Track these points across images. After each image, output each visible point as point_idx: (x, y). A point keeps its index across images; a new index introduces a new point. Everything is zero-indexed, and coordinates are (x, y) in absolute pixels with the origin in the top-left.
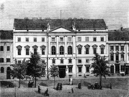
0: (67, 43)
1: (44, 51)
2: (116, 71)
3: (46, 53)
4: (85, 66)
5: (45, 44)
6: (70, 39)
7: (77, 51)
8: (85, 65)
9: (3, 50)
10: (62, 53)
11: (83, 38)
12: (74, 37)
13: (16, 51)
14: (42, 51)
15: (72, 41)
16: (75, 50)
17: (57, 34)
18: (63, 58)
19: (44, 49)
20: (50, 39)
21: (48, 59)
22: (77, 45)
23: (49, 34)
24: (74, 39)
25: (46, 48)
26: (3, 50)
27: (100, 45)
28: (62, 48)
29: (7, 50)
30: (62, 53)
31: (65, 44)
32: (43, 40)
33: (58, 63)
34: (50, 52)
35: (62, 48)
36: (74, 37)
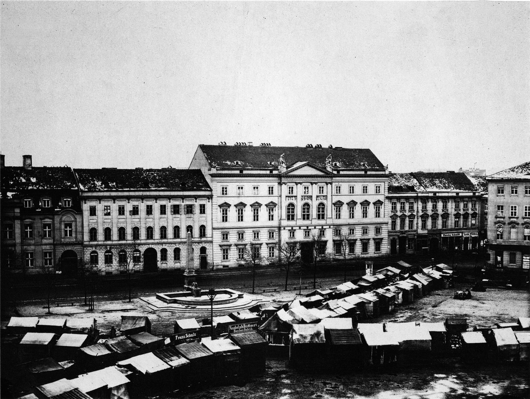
0: (317, 196)
1: (271, 213)
2: (162, 260)
3: (276, 218)
4: (266, 246)
5: (275, 200)
6: (321, 189)
7: (334, 213)
8: (267, 244)
9: (204, 213)
10: (306, 216)
11: (345, 187)
12: (329, 185)
13: (219, 214)
14: (270, 213)
15: (325, 194)
16: (330, 211)
17: (298, 180)
18: (309, 228)
19: (272, 210)
20: (285, 189)
21: (282, 228)
22: (333, 202)
23: (284, 180)
24: (328, 190)
25: (277, 206)
26: (204, 213)
27: (267, 203)
28: (306, 207)
29: (201, 213)
30: (306, 216)
31: (312, 200)
32: (271, 190)
33: (300, 236)
34: (284, 216)
35: (306, 207)
36: (329, 185)
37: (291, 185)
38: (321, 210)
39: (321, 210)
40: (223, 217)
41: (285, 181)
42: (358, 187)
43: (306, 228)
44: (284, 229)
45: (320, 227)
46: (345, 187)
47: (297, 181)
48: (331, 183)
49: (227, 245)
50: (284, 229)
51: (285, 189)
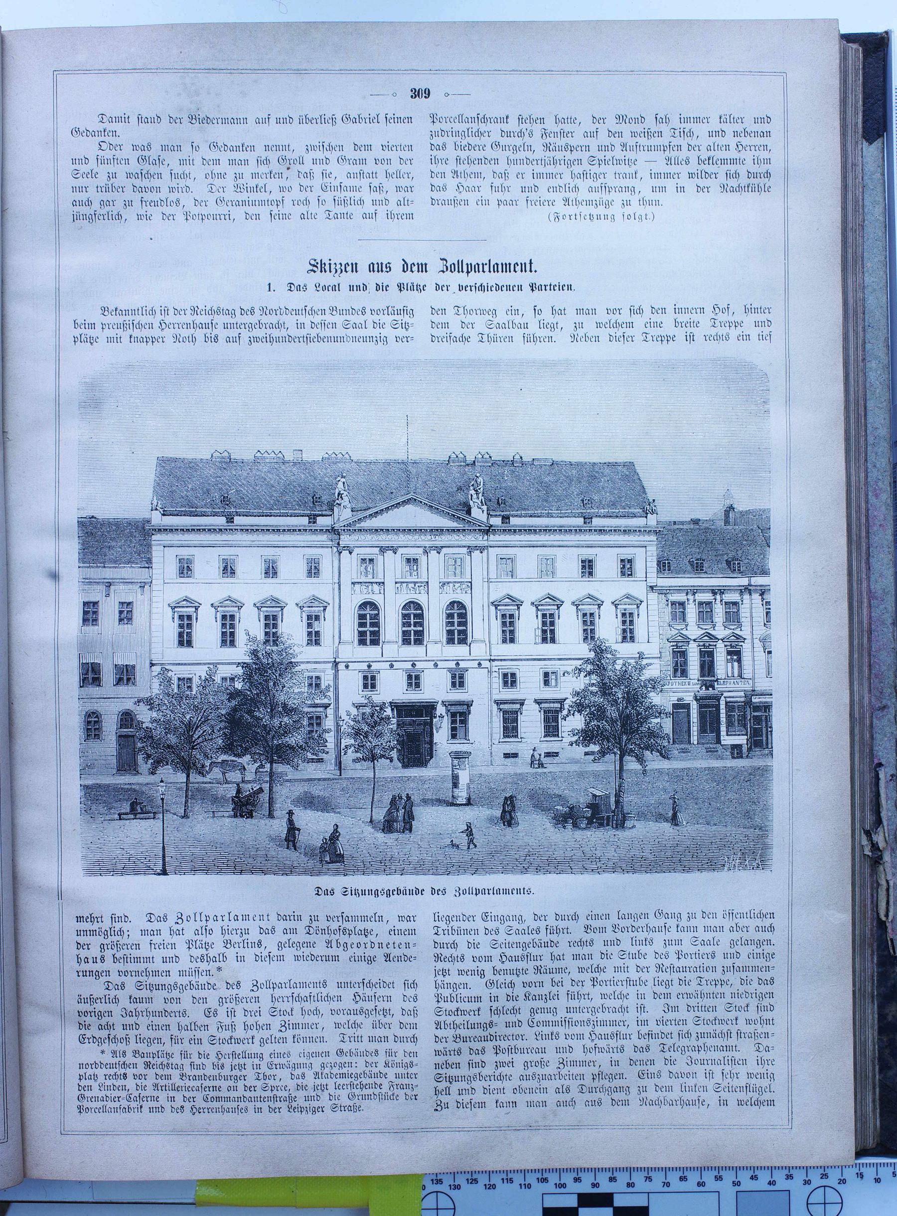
2: (702, 730)
8: (538, 702)
16: (483, 625)
21: (341, 666)
22: (491, 600)
23: (345, 540)
32: (313, 570)
37: (412, 552)
38: (456, 620)
39: (456, 620)
40: (224, 634)
41: (351, 544)
42: (568, 562)
43: (408, 665)
44: (347, 667)
45: (408, 665)
46: (527, 561)
47: (382, 544)
48: (439, 549)
49: (513, 702)
50: (347, 667)
51: (350, 564)
